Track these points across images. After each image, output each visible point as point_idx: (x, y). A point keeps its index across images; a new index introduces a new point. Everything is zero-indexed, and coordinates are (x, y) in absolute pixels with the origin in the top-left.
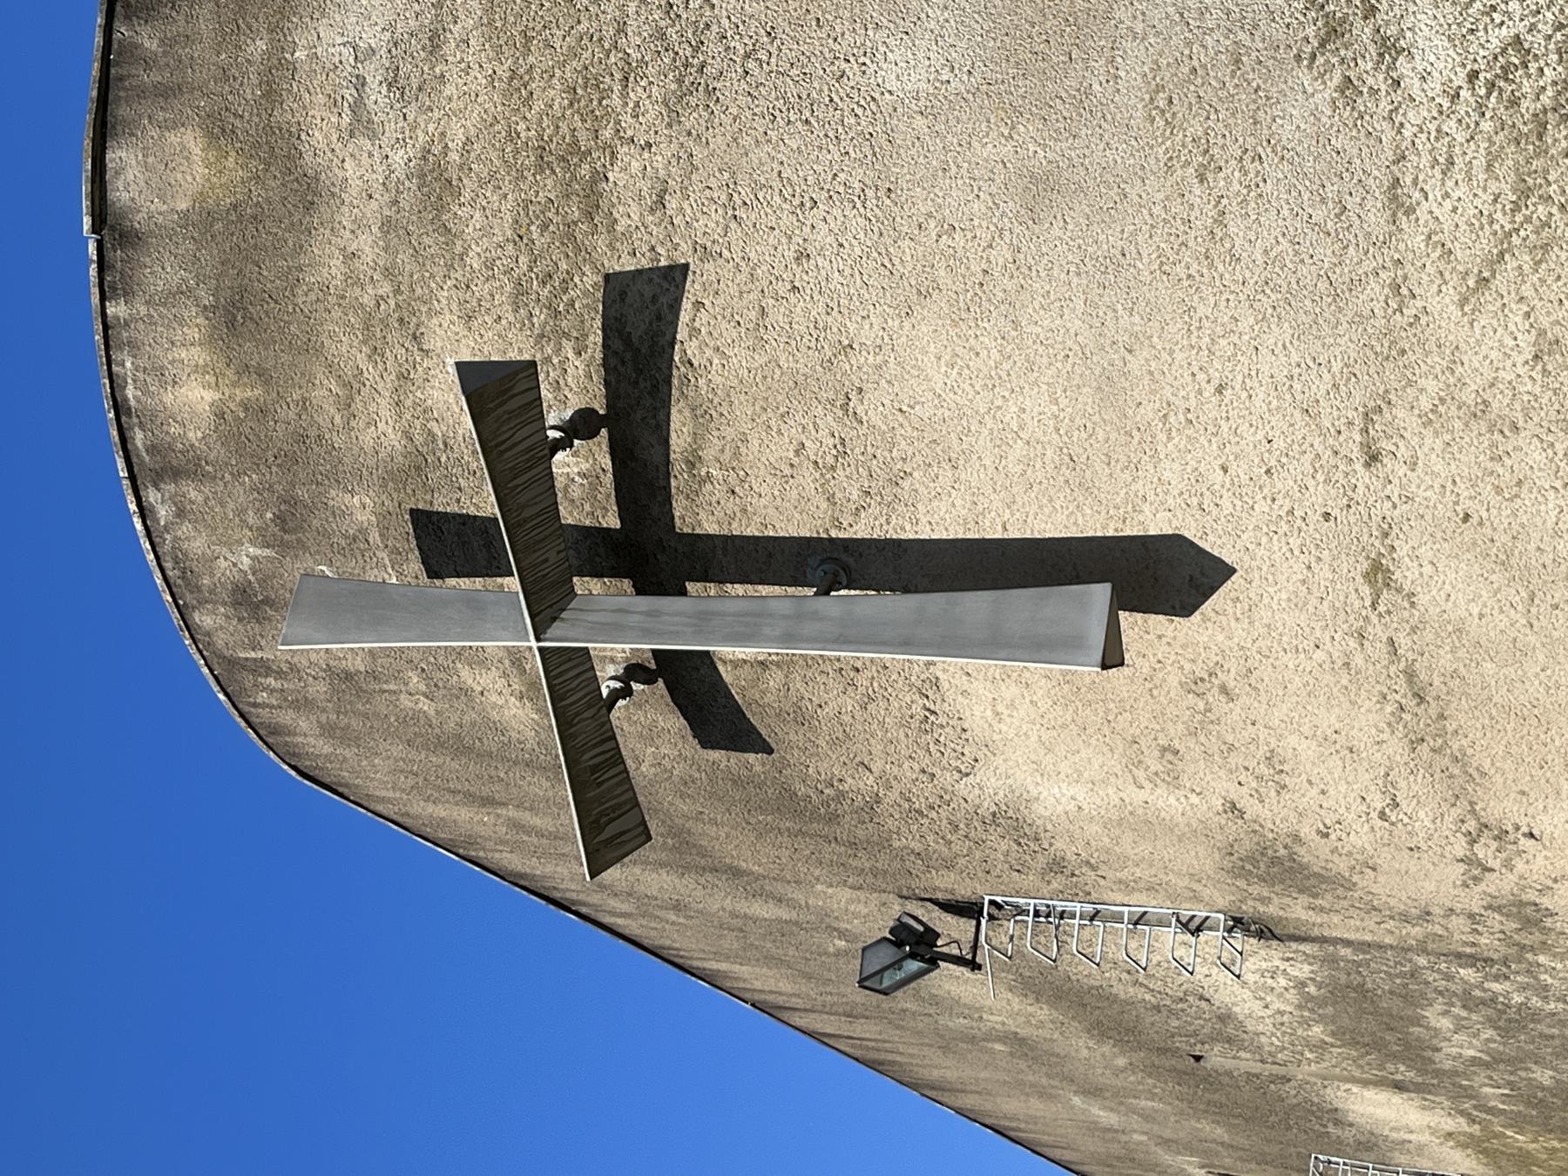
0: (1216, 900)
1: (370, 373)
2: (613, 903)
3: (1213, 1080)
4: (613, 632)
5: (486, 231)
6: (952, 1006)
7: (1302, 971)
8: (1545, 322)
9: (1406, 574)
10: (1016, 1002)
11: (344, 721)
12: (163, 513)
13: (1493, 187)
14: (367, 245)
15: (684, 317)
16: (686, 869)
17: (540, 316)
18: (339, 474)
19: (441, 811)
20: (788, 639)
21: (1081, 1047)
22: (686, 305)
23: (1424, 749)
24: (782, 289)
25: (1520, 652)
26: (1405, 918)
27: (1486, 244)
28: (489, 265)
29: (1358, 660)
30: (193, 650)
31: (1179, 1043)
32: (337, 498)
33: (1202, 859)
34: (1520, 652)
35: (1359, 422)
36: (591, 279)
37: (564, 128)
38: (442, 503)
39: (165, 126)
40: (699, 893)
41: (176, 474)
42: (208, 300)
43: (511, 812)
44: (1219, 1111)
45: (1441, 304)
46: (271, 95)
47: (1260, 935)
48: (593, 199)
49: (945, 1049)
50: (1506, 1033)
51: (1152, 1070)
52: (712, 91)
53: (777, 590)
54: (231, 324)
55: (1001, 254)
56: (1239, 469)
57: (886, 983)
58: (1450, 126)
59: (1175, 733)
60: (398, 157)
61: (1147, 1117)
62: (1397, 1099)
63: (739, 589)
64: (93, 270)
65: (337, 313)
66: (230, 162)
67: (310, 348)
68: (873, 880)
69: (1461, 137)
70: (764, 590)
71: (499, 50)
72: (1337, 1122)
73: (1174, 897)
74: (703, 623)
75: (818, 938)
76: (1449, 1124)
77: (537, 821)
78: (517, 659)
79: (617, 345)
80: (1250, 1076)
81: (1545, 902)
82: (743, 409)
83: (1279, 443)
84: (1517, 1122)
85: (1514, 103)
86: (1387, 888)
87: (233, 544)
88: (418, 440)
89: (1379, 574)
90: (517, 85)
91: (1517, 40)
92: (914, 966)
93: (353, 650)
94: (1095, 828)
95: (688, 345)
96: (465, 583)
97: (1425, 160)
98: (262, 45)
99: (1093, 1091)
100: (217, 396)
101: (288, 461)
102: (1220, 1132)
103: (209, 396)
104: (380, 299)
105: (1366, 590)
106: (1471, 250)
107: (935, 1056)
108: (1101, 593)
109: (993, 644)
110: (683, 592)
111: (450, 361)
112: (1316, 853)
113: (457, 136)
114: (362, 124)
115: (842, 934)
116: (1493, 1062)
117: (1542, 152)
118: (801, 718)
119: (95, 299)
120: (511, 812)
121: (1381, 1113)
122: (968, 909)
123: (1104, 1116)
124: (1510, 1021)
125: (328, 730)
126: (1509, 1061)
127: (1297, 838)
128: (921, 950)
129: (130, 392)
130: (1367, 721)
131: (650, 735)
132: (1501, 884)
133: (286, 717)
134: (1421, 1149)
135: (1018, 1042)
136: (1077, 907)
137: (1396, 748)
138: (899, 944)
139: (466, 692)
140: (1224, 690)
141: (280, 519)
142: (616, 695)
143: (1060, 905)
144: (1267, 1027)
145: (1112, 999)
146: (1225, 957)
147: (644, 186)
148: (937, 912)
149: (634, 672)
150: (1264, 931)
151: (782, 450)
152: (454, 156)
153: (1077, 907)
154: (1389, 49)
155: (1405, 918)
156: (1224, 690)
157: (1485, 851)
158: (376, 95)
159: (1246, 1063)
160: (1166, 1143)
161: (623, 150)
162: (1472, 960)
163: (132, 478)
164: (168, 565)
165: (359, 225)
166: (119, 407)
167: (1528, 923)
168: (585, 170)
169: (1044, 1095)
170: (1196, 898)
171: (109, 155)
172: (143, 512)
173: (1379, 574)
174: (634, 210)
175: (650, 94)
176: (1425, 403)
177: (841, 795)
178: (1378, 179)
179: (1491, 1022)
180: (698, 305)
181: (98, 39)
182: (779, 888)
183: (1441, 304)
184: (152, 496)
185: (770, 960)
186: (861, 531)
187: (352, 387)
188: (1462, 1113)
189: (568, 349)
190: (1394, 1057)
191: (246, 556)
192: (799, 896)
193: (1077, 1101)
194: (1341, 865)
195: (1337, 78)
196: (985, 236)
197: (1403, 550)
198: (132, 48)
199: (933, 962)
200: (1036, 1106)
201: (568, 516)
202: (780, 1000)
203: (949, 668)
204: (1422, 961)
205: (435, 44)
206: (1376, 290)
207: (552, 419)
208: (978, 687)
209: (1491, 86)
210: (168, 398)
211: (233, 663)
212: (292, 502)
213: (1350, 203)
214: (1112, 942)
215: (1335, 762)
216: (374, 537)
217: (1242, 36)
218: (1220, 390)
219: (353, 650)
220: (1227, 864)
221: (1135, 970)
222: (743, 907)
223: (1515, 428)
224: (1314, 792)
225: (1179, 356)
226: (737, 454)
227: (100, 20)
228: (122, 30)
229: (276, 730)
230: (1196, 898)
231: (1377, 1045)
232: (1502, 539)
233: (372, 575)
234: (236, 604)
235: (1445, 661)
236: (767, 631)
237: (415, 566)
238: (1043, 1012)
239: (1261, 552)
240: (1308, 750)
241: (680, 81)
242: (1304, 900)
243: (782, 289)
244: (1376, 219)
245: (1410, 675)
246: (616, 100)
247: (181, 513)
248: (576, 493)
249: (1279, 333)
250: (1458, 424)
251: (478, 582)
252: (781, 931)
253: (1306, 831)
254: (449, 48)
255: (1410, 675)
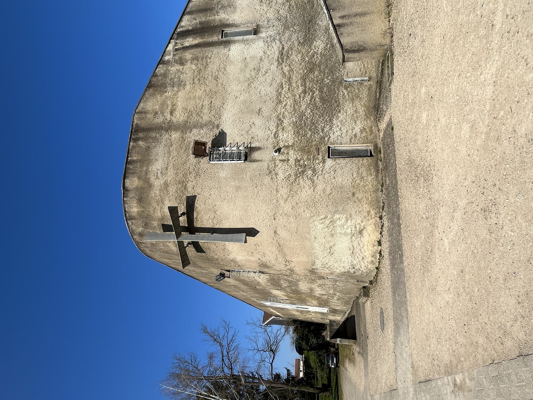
0: (258, 269)
1: (157, 207)
2: (186, 271)
3: (257, 290)
4: (186, 239)
5: (172, 191)
6: (227, 282)
7: (267, 277)
8: (293, 205)
9: (278, 232)
10: (235, 281)
11: (152, 249)
12: (130, 224)
13: (287, 190)
14: (157, 192)
15: (196, 201)
16: (195, 267)
17: (178, 201)
18: (153, 219)
19: (164, 260)
20: (207, 240)
21: (242, 286)
22: (196, 200)
23: (280, 252)
24: (208, 198)
25: (291, 241)
26: (278, 271)
27: (287, 196)
28: (172, 195)
29: (273, 242)
30: (133, 241)
31: (253, 286)
32: (152, 222)
33: (256, 265)
34: (291, 241)
35: (273, 215)
36: (185, 197)
37: (182, 179)
38: (166, 223)
39: (132, 177)
40: (196, 270)
41: (132, 219)
42: (137, 198)
43: (173, 260)
44: (258, 293)
45: (282, 202)
46: (146, 174)
47: (262, 273)
48: (185, 188)
49: (226, 287)
50: (289, 283)
51: (250, 289)
52: (200, 176)
53: (206, 234)
54: (140, 201)
55: (233, 195)
56: (260, 220)
57: (219, 280)
58: (283, 183)
59: (252, 250)
60: (162, 182)
61: (249, 294)
62: (278, 291)
63: (202, 234)
64: (122, 194)
65: (153, 200)
66: (141, 182)
67: (150, 204)
68: (217, 268)
69: (284, 184)
70: (205, 234)
71: (174, 170)
72: (271, 294)
73: (253, 269)
74: (197, 238)
75: (211, 275)
76: (283, 294)
77: (176, 261)
78: (174, 242)
79: (188, 204)
80: (261, 289)
81: (293, 269)
82: (203, 212)
83: (264, 217)
84: (291, 293)
85: (289, 181)
86: (277, 268)
87: (139, 228)
88: (163, 215)
89: (275, 232)
90: (177, 174)
91: (290, 174)
92: (222, 278)
93: (154, 241)
94: (244, 261)
95: (196, 205)
96: (168, 233)
97: (280, 187)
98: (145, 168)
99: (243, 291)
100: (137, 210)
101: (146, 218)
102: (258, 295)
103: (137, 210)
104: (159, 199)
105: (274, 234)
106: (285, 197)
107: (225, 288)
108: (245, 234)
109: (232, 240)
110: (195, 234)
111: (167, 206)
112: (268, 264)
113: (169, 180)
114: (157, 178)
115: (214, 274)
116: (289, 286)
117: (292, 186)
118: (209, 249)
119: (123, 198)
120: (173, 260)
121: (276, 293)
122: (229, 271)
123: (244, 294)
124: (290, 282)
125: (150, 251)
126: (290, 286)
127: (266, 262)
128: (223, 276)
129: (126, 209)
130: (274, 249)
131: (190, 251)
132: (289, 267)
133: (145, 249)
134: (280, 297)
135: (234, 286)
136: (242, 270)
137: (277, 252)
138: (220, 275)
139: (168, 246)
140: (258, 245)
141: (145, 225)
142: (186, 246)
143: (240, 270)
144: (263, 283)
145: (246, 281)
146: (258, 276)
147: (192, 186)
148: (225, 271)
149: (189, 243)
150: (263, 273)
151: (207, 217)
152: (169, 182)
153: (242, 270)
154: (276, 174)
155: (278, 271)
156: (258, 245)
157: (287, 263)
158: (159, 174)
159: (261, 287)
160: (252, 297)
161: (189, 182)
162: (286, 275)
163: (126, 219)
164: (130, 230)
165: (157, 190)
166: (125, 211)
167: (292, 271)
168: (184, 184)
169: (238, 292)
170: (255, 269)
171: (125, 181)
172: (127, 224)
173: (275, 232)
174: (190, 189)
175: (193, 175)
176: (280, 213)
177: (214, 258)
178: (275, 188)
179: (288, 282)
180: (198, 200)
181: (125, 167)
182: (206, 269)
183: (282, 202)
184: (129, 222)
185: (205, 277)
186: (217, 227)
187: (155, 209)
188: (285, 292)
189: (182, 205)
190: (278, 286)
191: (140, 229)
192: (208, 269)
193: (242, 292)
194: (271, 265)
195: (271, 177)
196: (231, 193)
197: (278, 230)
198: (129, 168)
199: (225, 277)
200: (237, 293)
201: (181, 225)
202: (206, 282)
203: (227, 243)
204: (280, 276)
205: (167, 169)
206: (275, 201)
207: (179, 213)
208: (230, 245)
209: (287, 179)
210: (131, 210)
211: (138, 242)
212: (147, 223)
213: (272, 191)
214: (245, 275)
215: (271, 254)
216: (157, 227)
217: (260, 172)
218: (258, 211)
219: (154, 241)
220: (259, 265)
221: (249, 278)
222: (202, 271)
223: (290, 216)
224: (268, 257)
225: (253, 207)
226: (202, 218)
227: (125, 164)
228: (128, 166)
229: (143, 250)
230: (255, 269)
231: (275, 285)
232: (289, 228)
233: (156, 232)
234: (139, 235)
235: (283, 242)
236: (205, 239)
237: (162, 230)
238: (238, 282)
239: (263, 230)
240: (268, 252)
241: (196, 174)
242: (267, 269)
243: (208, 198)
244: (275, 192)
245: (279, 244)
246: (188, 176)
247: (132, 224)
248: (182, 222)
249: (264, 205)
250: (284, 216)
251: (169, 233)
252: (206, 274)
253: (268, 262)
254: (168, 169)
255: (279, 244)
